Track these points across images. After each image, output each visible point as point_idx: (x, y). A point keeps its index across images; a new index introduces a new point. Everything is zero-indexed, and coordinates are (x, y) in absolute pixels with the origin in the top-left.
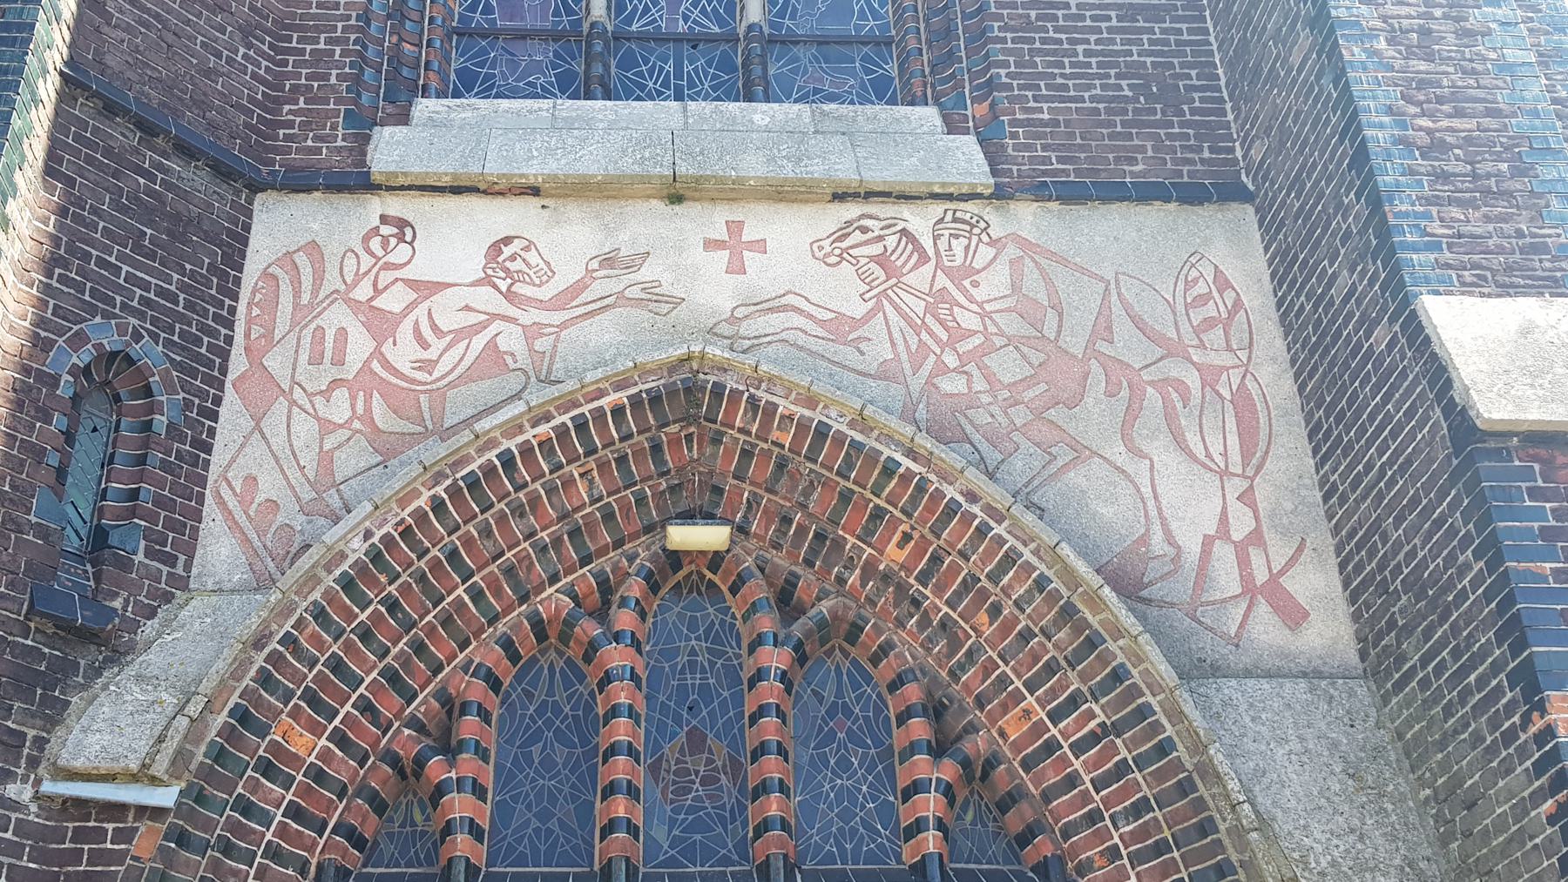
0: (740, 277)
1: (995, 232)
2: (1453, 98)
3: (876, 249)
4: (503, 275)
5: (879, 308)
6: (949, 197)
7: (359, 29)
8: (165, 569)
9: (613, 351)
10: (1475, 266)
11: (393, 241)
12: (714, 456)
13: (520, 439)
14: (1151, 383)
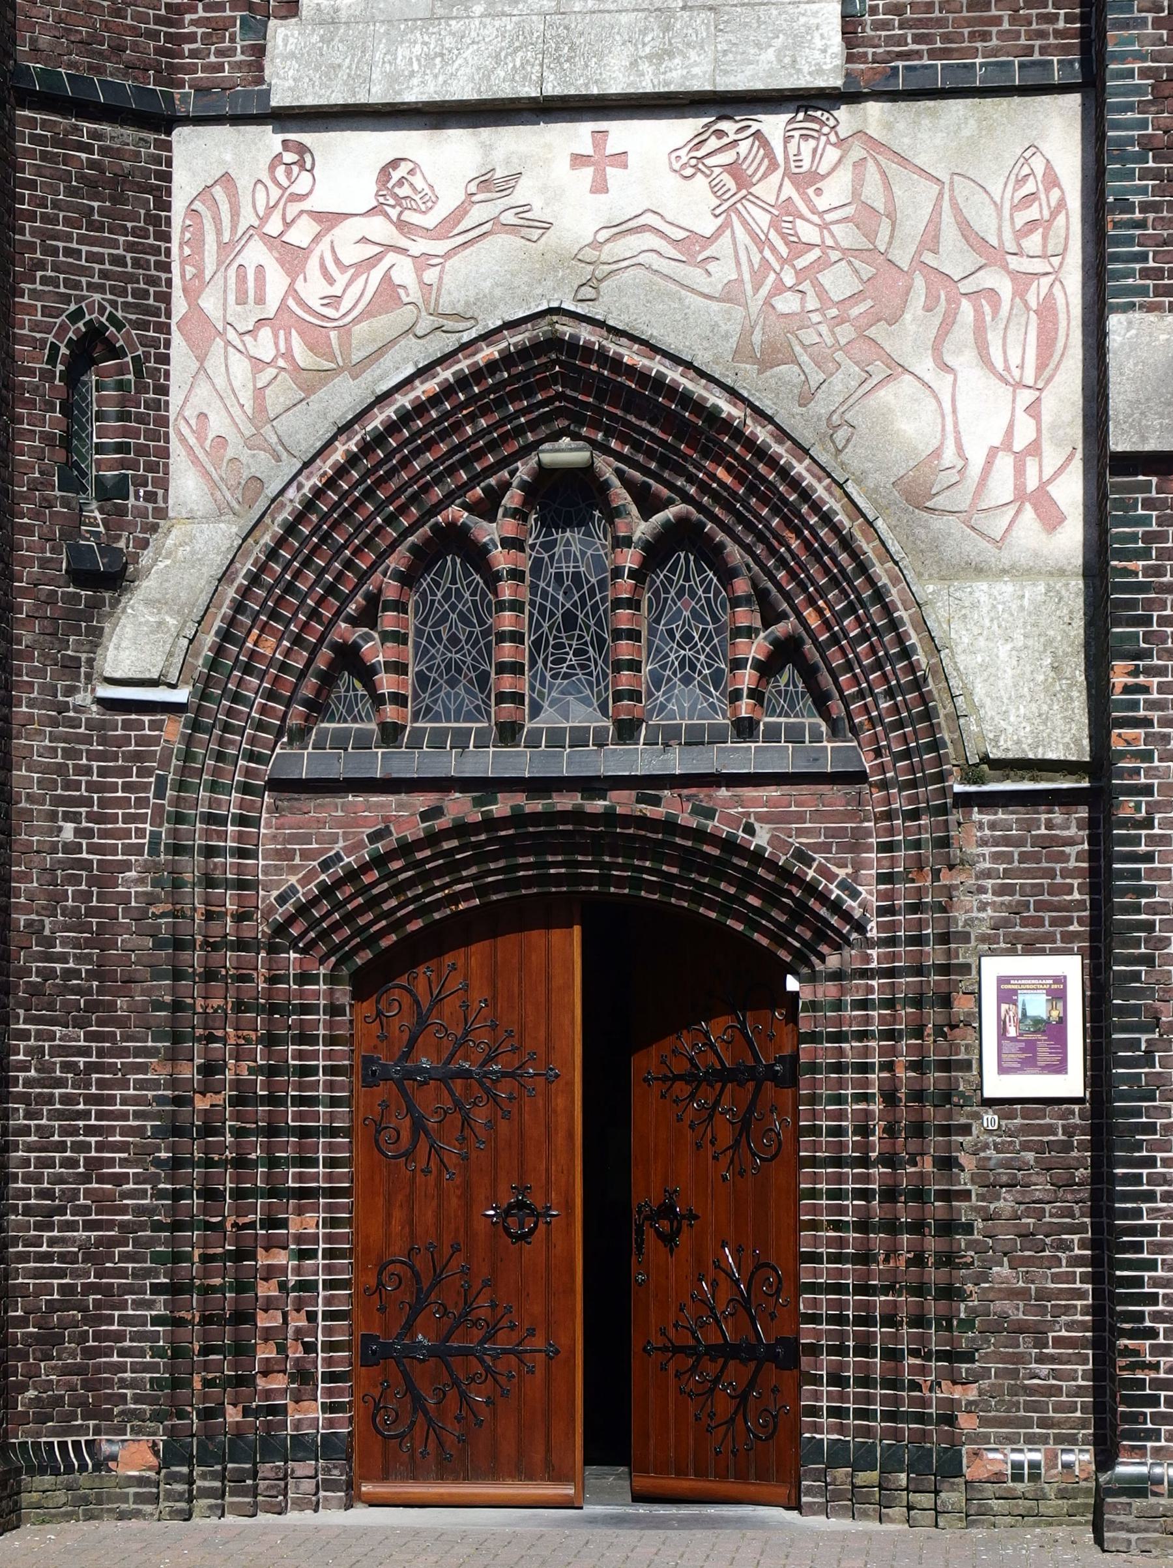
1: (843, 131)
3: (727, 158)
4: (392, 202)
5: (727, 224)
11: (295, 169)
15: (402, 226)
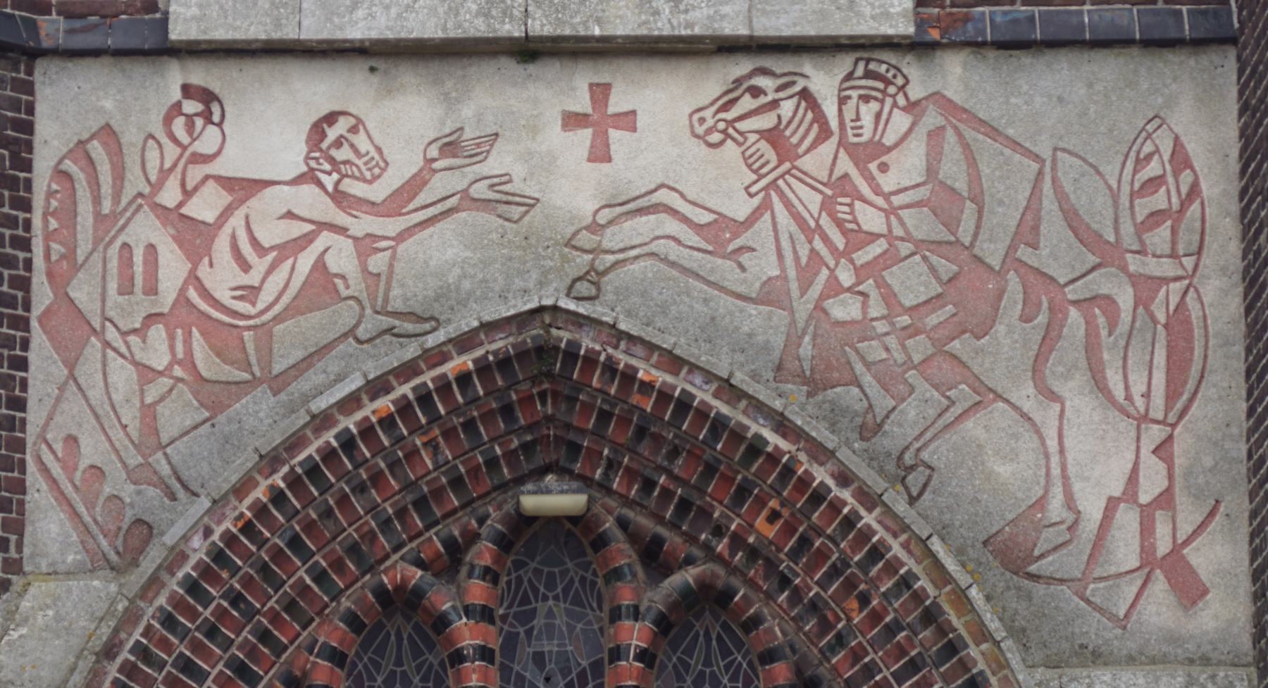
0: (605, 167)
1: (915, 92)
4: (327, 167)
5: (766, 206)
9: (457, 271)
11: (199, 122)
13: (359, 416)
14: (1075, 303)
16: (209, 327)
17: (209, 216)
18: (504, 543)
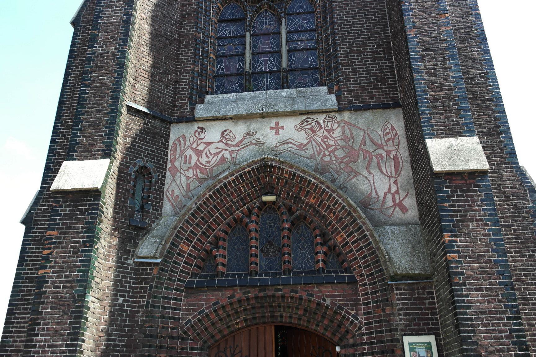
1: (338, 120)
2: (441, 86)
3: (310, 126)
5: (310, 141)
6: (327, 112)
7: (191, 81)
8: (156, 212)
10: (441, 130)
12: (272, 180)
13: (228, 180)
15: (226, 144)
16: (201, 169)
17: (202, 149)
18: (260, 209)
